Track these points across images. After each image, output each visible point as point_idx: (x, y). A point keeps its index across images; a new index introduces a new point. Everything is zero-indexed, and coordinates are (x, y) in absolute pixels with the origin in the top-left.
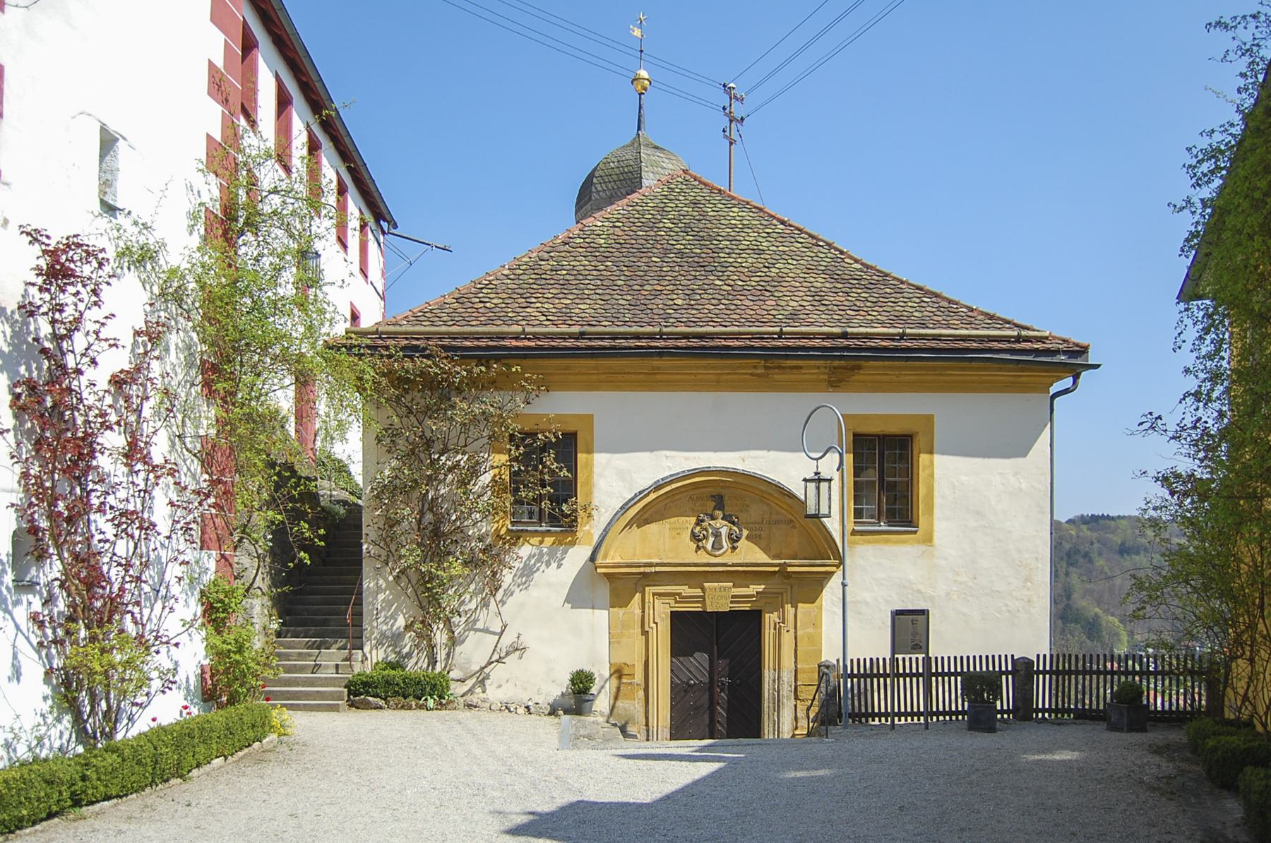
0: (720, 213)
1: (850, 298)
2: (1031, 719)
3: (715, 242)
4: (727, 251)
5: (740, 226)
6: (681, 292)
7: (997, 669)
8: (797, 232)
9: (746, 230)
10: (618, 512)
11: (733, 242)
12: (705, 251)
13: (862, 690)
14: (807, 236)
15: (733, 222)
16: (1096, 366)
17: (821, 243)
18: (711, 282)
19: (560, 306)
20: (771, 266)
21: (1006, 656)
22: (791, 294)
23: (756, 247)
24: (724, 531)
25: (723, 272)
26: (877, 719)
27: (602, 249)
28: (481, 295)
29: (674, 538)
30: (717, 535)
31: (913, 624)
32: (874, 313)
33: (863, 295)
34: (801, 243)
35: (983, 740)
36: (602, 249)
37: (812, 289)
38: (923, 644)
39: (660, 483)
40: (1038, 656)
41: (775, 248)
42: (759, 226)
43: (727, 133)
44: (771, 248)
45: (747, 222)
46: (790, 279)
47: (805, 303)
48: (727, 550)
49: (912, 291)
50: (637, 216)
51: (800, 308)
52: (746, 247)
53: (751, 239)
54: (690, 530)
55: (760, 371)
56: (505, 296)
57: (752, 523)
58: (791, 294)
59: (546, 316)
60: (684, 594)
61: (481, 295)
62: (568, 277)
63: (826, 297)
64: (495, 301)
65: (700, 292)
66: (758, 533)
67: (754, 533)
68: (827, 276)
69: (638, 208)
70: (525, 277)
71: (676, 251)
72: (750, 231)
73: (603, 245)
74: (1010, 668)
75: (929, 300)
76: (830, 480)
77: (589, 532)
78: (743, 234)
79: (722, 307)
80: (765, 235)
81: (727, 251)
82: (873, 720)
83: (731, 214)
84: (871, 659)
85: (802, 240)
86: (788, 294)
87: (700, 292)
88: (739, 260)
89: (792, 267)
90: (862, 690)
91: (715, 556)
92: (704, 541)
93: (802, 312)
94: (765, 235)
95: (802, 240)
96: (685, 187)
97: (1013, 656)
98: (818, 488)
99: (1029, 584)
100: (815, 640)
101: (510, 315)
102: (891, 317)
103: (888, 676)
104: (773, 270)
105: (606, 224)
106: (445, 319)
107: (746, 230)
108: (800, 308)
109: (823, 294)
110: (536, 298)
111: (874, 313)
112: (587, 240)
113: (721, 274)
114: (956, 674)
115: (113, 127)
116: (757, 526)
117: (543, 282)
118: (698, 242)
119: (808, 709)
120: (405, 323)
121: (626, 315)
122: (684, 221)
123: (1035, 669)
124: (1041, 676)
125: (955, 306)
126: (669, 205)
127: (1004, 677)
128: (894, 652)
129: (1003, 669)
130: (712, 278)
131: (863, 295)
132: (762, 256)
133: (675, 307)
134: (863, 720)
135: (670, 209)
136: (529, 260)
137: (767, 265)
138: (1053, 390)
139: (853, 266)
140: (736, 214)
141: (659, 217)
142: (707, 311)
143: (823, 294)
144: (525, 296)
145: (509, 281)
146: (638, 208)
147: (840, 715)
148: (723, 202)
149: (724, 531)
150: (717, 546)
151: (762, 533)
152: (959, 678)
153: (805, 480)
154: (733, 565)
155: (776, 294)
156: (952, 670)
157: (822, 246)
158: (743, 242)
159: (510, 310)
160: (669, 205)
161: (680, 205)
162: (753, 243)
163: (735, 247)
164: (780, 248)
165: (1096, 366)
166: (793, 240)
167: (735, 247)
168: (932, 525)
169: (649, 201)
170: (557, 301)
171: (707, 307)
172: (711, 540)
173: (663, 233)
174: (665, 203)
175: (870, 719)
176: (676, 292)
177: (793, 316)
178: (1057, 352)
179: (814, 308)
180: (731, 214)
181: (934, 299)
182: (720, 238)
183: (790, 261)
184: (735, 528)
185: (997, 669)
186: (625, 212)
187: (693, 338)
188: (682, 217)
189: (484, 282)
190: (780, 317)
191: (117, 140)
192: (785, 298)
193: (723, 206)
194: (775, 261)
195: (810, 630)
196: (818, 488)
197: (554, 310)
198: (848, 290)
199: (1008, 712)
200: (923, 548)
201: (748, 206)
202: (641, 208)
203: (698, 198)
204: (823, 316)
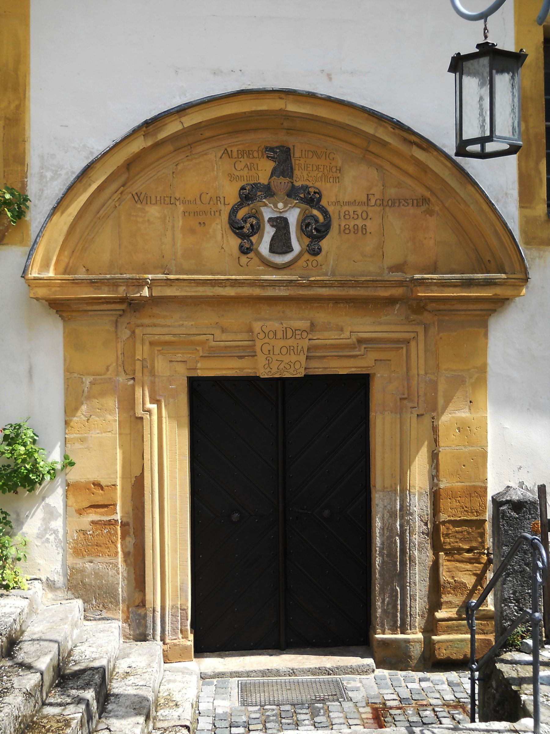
29: (193, 231)
54: (225, 217)
57: (349, 203)
66: (360, 223)
67: (352, 223)
91: (278, 268)
92: (254, 239)
116: (359, 210)
151: (368, 223)
172: (269, 232)
184: (315, 212)
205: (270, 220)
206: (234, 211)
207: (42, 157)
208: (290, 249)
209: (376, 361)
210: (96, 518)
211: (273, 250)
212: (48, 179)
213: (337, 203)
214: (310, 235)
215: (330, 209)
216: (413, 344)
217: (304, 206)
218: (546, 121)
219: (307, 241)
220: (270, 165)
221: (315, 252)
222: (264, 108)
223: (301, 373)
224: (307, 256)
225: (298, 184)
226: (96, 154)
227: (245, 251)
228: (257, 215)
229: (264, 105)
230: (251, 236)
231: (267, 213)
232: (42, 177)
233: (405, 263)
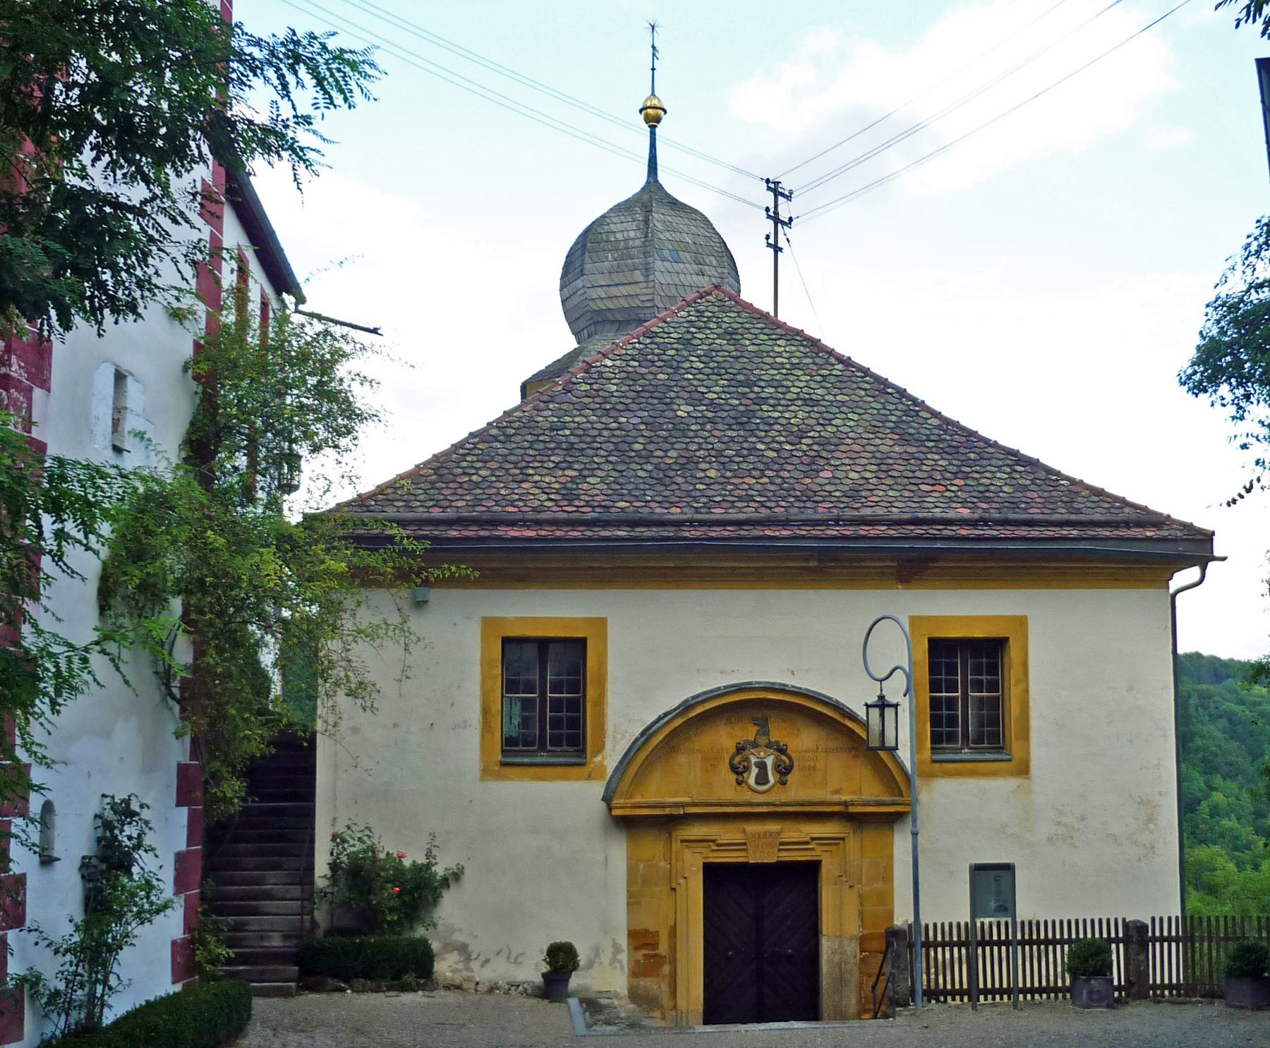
0: (762, 348)
1: (924, 467)
2: (1146, 996)
3: (756, 389)
4: (772, 402)
5: (788, 366)
6: (714, 459)
7: (1105, 935)
8: (859, 374)
9: (795, 372)
10: (637, 740)
11: (780, 390)
12: (744, 401)
13: (948, 962)
14: (872, 380)
15: (779, 360)
16: (1224, 559)
17: (889, 390)
18: (752, 445)
19: (563, 480)
20: (827, 422)
21: (1116, 920)
22: (851, 462)
23: (807, 396)
24: (770, 762)
25: (766, 431)
26: (958, 998)
27: (613, 400)
28: (465, 464)
30: (762, 766)
31: (996, 880)
32: (953, 488)
33: (941, 463)
34: (865, 390)
35: (1098, 1022)
36: (613, 400)
37: (878, 455)
38: (1009, 905)
39: (690, 703)
40: (1153, 919)
41: (831, 398)
42: (811, 366)
43: (771, 241)
44: (827, 398)
45: (797, 361)
46: (850, 441)
47: (868, 475)
48: (774, 785)
49: (1002, 456)
50: (657, 351)
51: (862, 482)
52: (795, 396)
53: (802, 384)
54: (727, 761)
55: (812, 564)
56: (495, 465)
58: (851, 462)
59: (548, 494)
60: (720, 842)
61: (465, 464)
62: (572, 439)
63: (895, 467)
64: (482, 472)
65: (738, 459)
66: (812, 763)
68: (897, 437)
69: (658, 340)
70: (518, 438)
71: (706, 402)
72: (800, 373)
73: (615, 394)
74: (1121, 935)
75: (1023, 469)
76: (896, 706)
77: (601, 764)
78: (792, 378)
79: (765, 480)
80: (819, 378)
81: (772, 402)
82: (954, 999)
83: (777, 349)
84: (959, 924)
85: (867, 386)
86: (847, 461)
87: (738, 459)
88: (787, 415)
89: (852, 423)
90: (948, 962)
92: (745, 775)
93: (865, 487)
94: (819, 378)
95: (867, 386)
96: (717, 309)
97: (1124, 920)
98: (882, 715)
99: (1151, 826)
100: (885, 898)
101: (503, 492)
102: (974, 494)
103: (1019, 943)
104: (829, 428)
105: (618, 363)
106: (421, 497)
107: (795, 372)
108: (862, 482)
109: (891, 461)
110: (533, 468)
111: (953, 488)
112: (595, 387)
113: (763, 434)
114: (1062, 942)
115: (126, 365)
117: (541, 446)
118: (734, 389)
119: (874, 987)
120: (373, 503)
121: (647, 492)
122: (718, 359)
123: (1150, 934)
124: (1158, 945)
125: (1054, 478)
126: (698, 336)
127: (1113, 946)
128: (973, 916)
129: (1113, 935)
130: (754, 439)
131: (941, 463)
132: (815, 409)
133: (708, 481)
134: (942, 998)
135: (699, 342)
136: (522, 415)
137: (821, 422)
138: (1175, 584)
139: (929, 421)
140: (782, 349)
141: (685, 353)
142: (747, 487)
143: (891, 461)
144: (519, 465)
145: (499, 445)
146: (658, 340)
147: (912, 992)
148: (766, 331)
149: (770, 762)
150: (761, 779)
152: (1066, 947)
153: (868, 706)
154: (782, 805)
155: (832, 462)
156: (1166, 934)
157: (891, 394)
158: (792, 389)
159: (502, 485)
160: (698, 336)
161: (711, 336)
162: (804, 390)
163: (781, 396)
164: (838, 398)
165: (1224, 559)
166: (855, 386)
167: (781, 396)
168: (1028, 753)
169: (672, 330)
170: (560, 473)
171: (746, 480)
172: (755, 771)
173: (690, 377)
174: (693, 333)
175: (949, 998)
176: (708, 459)
177: (854, 494)
178: (1175, 540)
179: (880, 481)
180: (777, 349)
181: (1028, 469)
182: (763, 384)
183: (850, 416)
184: (784, 758)
185: (1105, 935)
186: (642, 346)
187: (730, 525)
188: (714, 354)
189: (468, 446)
190: (837, 494)
191: (126, 376)
192: (843, 468)
193: (766, 337)
194: (832, 416)
195: (879, 885)
196: (882, 715)
197: (557, 486)
198: (922, 456)
199: (1119, 988)
200: (1013, 782)
201: (799, 338)
202: (662, 340)
203: (735, 326)
204: (891, 493)
205: (755, 764)
206: (733, 758)
207: (615, 726)
208: (767, 782)
209: (507, 646)
210: (647, 952)
211: (757, 783)
212: (40, 511)
213: (796, 751)
214: (780, 773)
215: (793, 756)
216: (847, 841)
217: (776, 753)
218: (931, 691)
219: (778, 776)
220: (756, 728)
221: (784, 783)
222: (754, 697)
223: (774, 860)
224: (778, 785)
225: (773, 740)
226: (648, 723)
227: (739, 783)
228: (747, 759)
229: (753, 696)
230: (34, 790)
231: (753, 760)
232: (614, 738)
233: (841, 789)
